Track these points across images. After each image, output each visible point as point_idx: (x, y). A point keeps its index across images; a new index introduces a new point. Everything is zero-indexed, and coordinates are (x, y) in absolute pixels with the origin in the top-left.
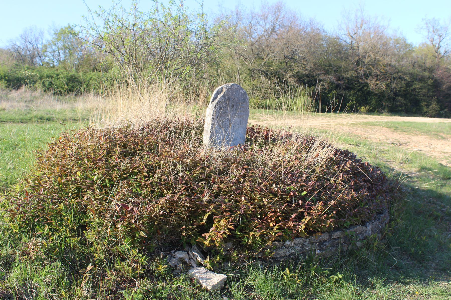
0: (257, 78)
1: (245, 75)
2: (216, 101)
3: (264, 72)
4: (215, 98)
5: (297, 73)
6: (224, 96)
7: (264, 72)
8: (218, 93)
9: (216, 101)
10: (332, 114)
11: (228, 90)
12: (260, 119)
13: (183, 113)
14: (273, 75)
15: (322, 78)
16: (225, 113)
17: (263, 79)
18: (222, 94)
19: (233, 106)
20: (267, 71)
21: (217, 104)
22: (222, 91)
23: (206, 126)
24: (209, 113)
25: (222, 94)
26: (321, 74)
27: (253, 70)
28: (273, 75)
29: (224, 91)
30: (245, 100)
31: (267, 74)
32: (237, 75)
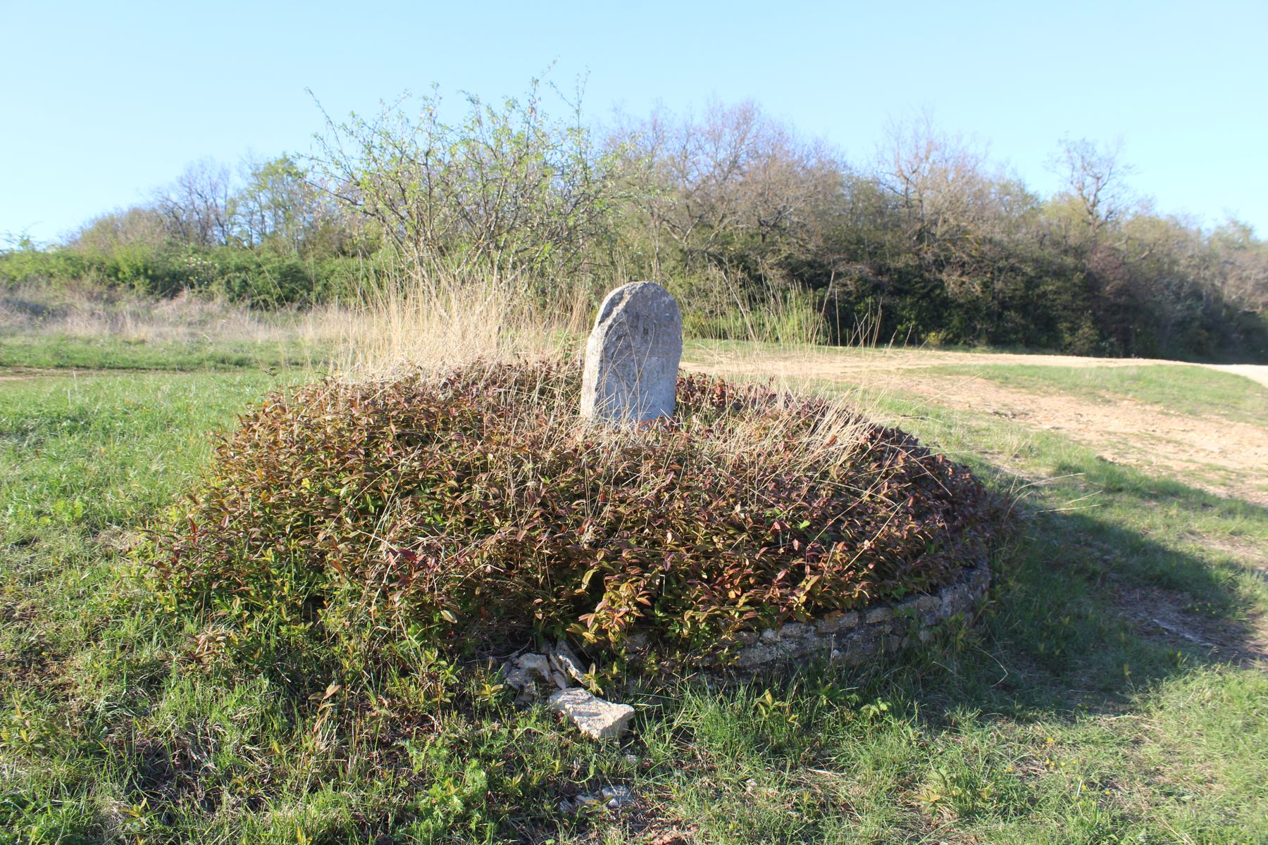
0: (699, 271)
1: (673, 263)
2: (609, 321)
3: (715, 257)
4: (606, 315)
5: (786, 258)
6: (625, 310)
7: (715, 257)
8: (613, 303)
9: (609, 321)
10: (861, 349)
11: (635, 296)
12: (706, 362)
13: (535, 347)
14: (735, 262)
15: (841, 269)
16: (629, 347)
17: (713, 271)
18: (622, 306)
19: (646, 332)
20: (721, 254)
21: (610, 327)
22: (621, 299)
23: (585, 376)
24: (593, 346)
25: (622, 306)
26: (840, 260)
27: (691, 252)
28: (735, 262)
29: (627, 297)
30: (672, 318)
31: (720, 262)
32: (654, 263)
